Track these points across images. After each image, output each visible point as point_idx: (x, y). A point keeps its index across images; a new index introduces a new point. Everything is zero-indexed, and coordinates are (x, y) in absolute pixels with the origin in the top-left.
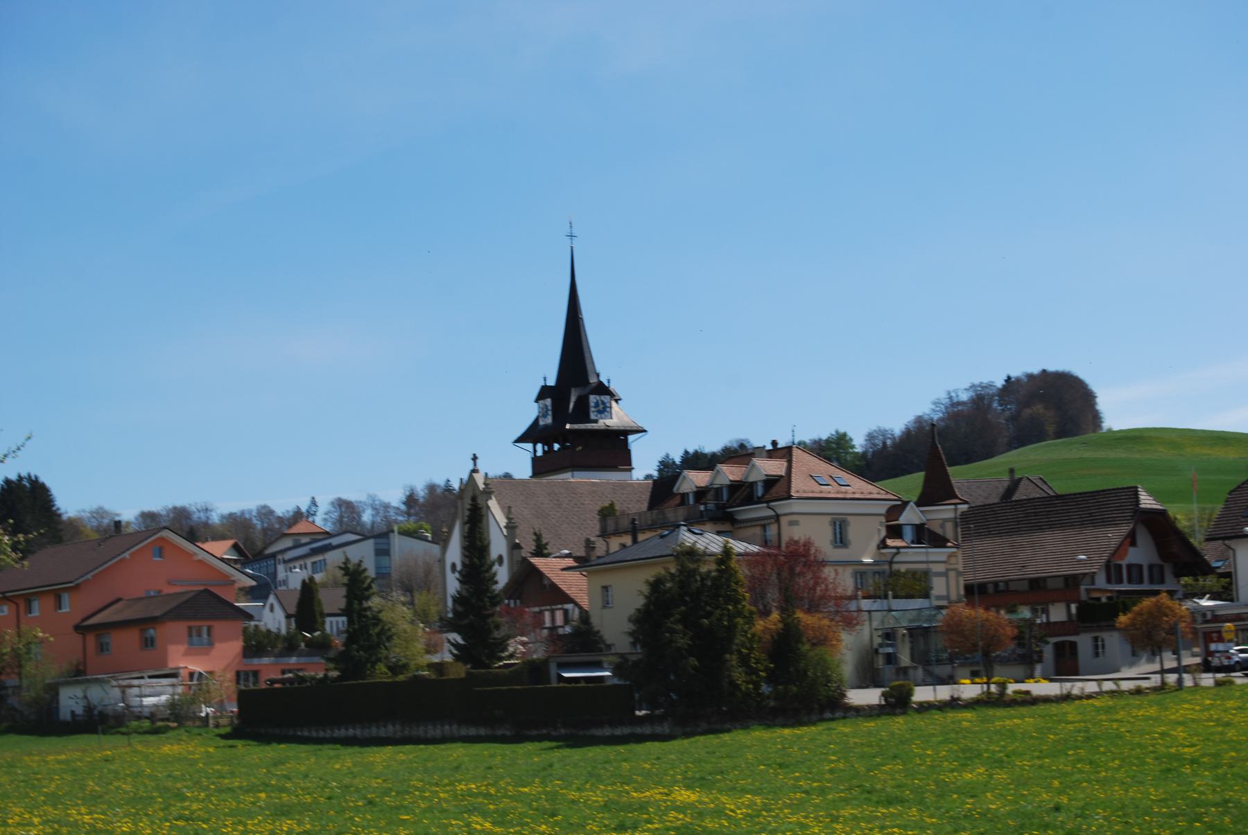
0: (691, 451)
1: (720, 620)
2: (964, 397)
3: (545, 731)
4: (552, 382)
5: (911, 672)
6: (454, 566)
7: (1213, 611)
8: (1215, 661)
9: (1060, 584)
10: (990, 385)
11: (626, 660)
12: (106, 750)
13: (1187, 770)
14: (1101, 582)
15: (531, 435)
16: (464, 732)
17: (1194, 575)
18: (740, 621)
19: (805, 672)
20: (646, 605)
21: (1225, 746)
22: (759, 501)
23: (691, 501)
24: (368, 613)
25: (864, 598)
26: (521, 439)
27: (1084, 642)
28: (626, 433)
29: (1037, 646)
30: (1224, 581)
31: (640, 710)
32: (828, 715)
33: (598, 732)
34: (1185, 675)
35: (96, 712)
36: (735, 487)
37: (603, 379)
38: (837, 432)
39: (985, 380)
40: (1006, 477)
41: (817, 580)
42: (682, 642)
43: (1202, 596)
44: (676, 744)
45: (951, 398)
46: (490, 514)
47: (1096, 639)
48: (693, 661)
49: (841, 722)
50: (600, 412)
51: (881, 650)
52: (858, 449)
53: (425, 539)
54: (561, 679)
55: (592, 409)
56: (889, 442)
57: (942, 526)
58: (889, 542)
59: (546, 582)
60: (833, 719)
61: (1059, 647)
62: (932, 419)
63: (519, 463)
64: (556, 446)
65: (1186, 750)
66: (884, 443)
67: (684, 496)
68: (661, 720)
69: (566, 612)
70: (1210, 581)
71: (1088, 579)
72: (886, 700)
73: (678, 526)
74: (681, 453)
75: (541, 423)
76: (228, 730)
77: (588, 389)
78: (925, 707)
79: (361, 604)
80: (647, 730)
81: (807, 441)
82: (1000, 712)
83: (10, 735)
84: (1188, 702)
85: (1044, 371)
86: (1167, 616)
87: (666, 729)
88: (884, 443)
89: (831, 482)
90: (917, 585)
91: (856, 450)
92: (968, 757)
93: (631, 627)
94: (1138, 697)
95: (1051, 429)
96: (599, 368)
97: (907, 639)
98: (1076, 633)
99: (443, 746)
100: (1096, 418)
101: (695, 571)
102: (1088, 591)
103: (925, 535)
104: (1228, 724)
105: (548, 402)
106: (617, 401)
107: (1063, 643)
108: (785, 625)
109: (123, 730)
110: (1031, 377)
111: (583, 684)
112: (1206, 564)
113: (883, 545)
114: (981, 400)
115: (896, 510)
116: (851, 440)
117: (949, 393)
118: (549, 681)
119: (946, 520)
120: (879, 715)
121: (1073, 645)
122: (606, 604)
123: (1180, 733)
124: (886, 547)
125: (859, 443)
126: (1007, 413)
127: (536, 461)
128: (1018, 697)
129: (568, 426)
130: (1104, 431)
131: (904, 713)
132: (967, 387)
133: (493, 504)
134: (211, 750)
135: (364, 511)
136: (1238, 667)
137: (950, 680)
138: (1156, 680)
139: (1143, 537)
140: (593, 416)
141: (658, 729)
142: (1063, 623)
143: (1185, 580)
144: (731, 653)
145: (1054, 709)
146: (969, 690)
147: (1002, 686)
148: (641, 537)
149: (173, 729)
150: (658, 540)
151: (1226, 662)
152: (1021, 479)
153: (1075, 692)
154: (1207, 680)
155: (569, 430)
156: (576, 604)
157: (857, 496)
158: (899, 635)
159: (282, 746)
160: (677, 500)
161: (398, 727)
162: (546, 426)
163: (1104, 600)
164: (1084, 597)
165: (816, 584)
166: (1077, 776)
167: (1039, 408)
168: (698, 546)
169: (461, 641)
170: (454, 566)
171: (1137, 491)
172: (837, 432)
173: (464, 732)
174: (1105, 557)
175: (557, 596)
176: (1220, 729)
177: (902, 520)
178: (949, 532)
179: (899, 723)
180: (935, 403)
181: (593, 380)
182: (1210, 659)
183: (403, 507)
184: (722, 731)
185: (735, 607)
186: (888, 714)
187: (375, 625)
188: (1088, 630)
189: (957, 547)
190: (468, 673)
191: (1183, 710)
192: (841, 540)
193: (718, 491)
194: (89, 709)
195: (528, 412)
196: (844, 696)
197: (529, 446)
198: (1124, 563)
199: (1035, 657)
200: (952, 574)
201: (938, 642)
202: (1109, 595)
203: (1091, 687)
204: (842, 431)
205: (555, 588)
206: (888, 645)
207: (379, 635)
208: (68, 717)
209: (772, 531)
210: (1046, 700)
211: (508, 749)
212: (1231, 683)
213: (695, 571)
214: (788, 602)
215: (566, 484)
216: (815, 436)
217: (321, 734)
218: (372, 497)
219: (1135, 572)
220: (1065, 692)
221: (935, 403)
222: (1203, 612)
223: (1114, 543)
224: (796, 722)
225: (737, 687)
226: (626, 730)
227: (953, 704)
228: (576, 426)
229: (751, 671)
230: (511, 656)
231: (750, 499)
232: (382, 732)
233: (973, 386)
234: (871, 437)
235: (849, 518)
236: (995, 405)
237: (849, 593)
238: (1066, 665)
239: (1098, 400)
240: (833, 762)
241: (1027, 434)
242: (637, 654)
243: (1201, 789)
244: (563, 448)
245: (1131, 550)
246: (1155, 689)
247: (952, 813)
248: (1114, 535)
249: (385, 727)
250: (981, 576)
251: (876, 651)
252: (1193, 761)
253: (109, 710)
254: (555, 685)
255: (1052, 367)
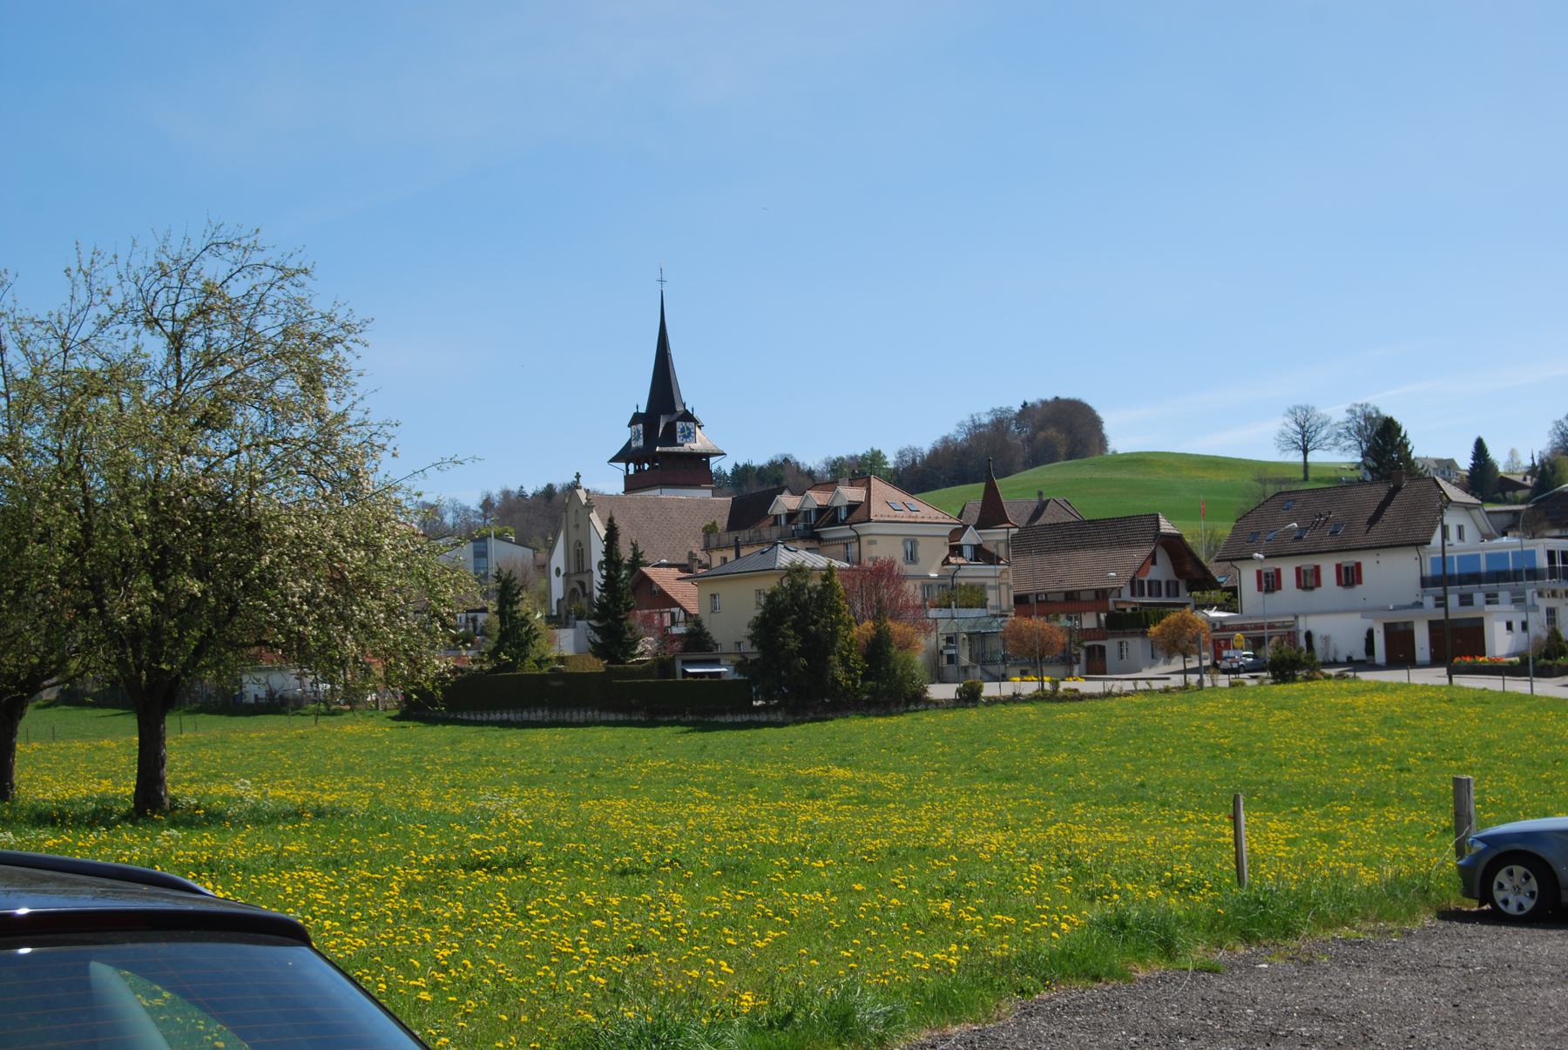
0: (741, 464)
1: (824, 627)
2: (986, 420)
3: (675, 718)
4: (643, 410)
5: (971, 670)
6: (558, 571)
7: (1221, 622)
8: (1224, 664)
9: (1092, 596)
10: (1009, 410)
11: (746, 659)
12: (298, 729)
13: (1228, 757)
14: (1126, 594)
15: (624, 456)
16: (604, 717)
17: (1203, 590)
18: (841, 627)
19: (894, 671)
20: (763, 614)
21: (1253, 738)
22: (843, 523)
23: (783, 522)
24: (518, 615)
25: (932, 607)
26: (614, 460)
27: (1111, 645)
28: (708, 455)
29: (1075, 650)
30: (1227, 594)
31: (757, 701)
32: (912, 707)
33: (721, 719)
34: (1204, 676)
35: (277, 696)
36: (821, 510)
37: (688, 408)
38: (872, 449)
39: (1004, 406)
40: (1036, 499)
41: (900, 593)
42: (793, 645)
43: (1210, 607)
44: (791, 730)
45: (973, 421)
46: (592, 528)
47: (1121, 644)
48: (803, 661)
49: (924, 714)
50: (686, 437)
51: (944, 652)
52: (891, 466)
53: (510, 541)
54: (685, 674)
55: (679, 434)
56: (918, 459)
57: (996, 546)
58: (952, 560)
59: (655, 588)
60: (917, 711)
61: (1090, 650)
62: (956, 440)
63: (610, 481)
64: (647, 466)
65: (1222, 740)
66: (914, 460)
67: (777, 517)
68: (776, 708)
69: (673, 615)
70: (1214, 595)
71: (1115, 593)
72: (960, 695)
73: (776, 544)
74: (732, 466)
75: (633, 445)
76: (397, 712)
77: (675, 417)
78: (992, 701)
79: (511, 607)
80: (763, 718)
81: (845, 457)
82: (1056, 707)
83: (202, 715)
84: (1212, 700)
85: (1057, 398)
86: (1190, 627)
87: (780, 717)
88: (914, 460)
89: (903, 507)
90: (975, 596)
91: (888, 466)
92: (1051, 746)
93: (751, 632)
94: (1167, 695)
95: (1062, 450)
96: (684, 399)
97: (967, 642)
98: (1105, 638)
99: (590, 729)
100: (1102, 442)
101: (804, 585)
102: (1115, 602)
103: (982, 554)
104: (1249, 720)
105: (640, 426)
106: (700, 427)
107: (1094, 646)
108: (878, 632)
109: (302, 711)
110: (1045, 403)
111: (707, 679)
112: (1213, 578)
113: (946, 562)
114: (1000, 423)
115: (957, 533)
116: (885, 457)
117: (972, 416)
118: (675, 677)
119: (998, 542)
120: (954, 708)
121: (1102, 649)
122: (714, 610)
123: (1209, 725)
124: (949, 564)
125: (891, 460)
126: (1023, 435)
127: (628, 478)
128: (1068, 694)
129: (658, 449)
130: (1110, 453)
131: (976, 706)
132: (988, 411)
133: (594, 516)
134: (387, 730)
135: (446, 513)
136: (1242, 669)
137: (1004, 678)
138: (1177, 680)
139: (1163, 558)
140: (679, 441)
141: (773, 717)
142: (1094, 630)
143: (1197, 594)
144: (834, 654)
145: (1100, 704)
146: (1029, 687)
147: (1055, 684)
148: (743, 552)
149: (347, 711)
150: (758, 556)
151: (1235, 665)
152: (1048, 501)
153: (1115, 690)
154: (1223, 681)
155: (659, 452)
156: (682, 608)
157: (925, 520)
158: (960, 639)
159: (447, 727)
160: (771, 520)
161: (546, 712)
162: (638, 449)
163: (1129, 610)
164: (1111, 607)
165: (898, 596)
166: (1144, 761)
167: (1052, 432)
168: (806, 565)
169: (599, 640)
170: (558, 571)
171: (1158, 518)
172: (872, 449)
173: (604, 717)
174: (1131, 574)
175: (666, 600)
176: (1244, 724)
177: (962, 541)
178: (1002, 552)
179: (973, 715)
180: (959, 425)
181: (679, 409)
182: (1218, 662)
183: (481, 511)
184: (826, 720)
185: (837, 616)
186: (962, 707)
187: (525, 625)
188: (1114, 636)
189: (1009, 564)
190: (607, 669)
191: (1208, 708)
192: (911, 557)
193: (808, 513)
194: (271, 693)
195: (621, 435)
196: (926, 691)
197: (623, 465)
198: (1146, 579)
199: (1074, 659)
200: (1004, 588)
201: (994, 645)
202: (1133, 606)
203: (1129, 686)
204: (876, 449)
205: (663, 594)
206: (951, 648)
207: (527, 633)
208: (252, 700)
209: (854, 548)
210: (1092, 697)
211: (649, 732)
212: (1243, 684)
213: (804, 585)
214: (879, 613)
215: (657, 500)
216: (851, 453)
217: (479, 717)
218: (454, 502)
219: (1155, 587)
220: (1107, 690)
221: (959, 425)
222: (1213, 623)
223: (1138, 563)
224: (888, 713)
225: (838, 683)
226: (746, 718)
227: (1015, 699)
228: (665, 449)
229: (850, 670)
230: (642, 654)
231: (834, 521)
232: (533, 717)
233: (993, 410)
234: (901, 454)
235: (919, 539)
236: (1013, 428)
237: (918, 602)
238: (1096, 665)
239: (1105, 425)
240: (939, 747)
241: (1039, 456)
242: (752, 652)
243: (1246, 772)
244: (652, 467)
245: (1153, 568)
246: (1179, 689)
247: (193, 774)
248: (1138, 555)
249: (535, 712)
250: (1024, 589)
251: (941, 652)
252: (1231, 751)
253: (289, 695)
254: (680, 678)
255: (1064, 395)
